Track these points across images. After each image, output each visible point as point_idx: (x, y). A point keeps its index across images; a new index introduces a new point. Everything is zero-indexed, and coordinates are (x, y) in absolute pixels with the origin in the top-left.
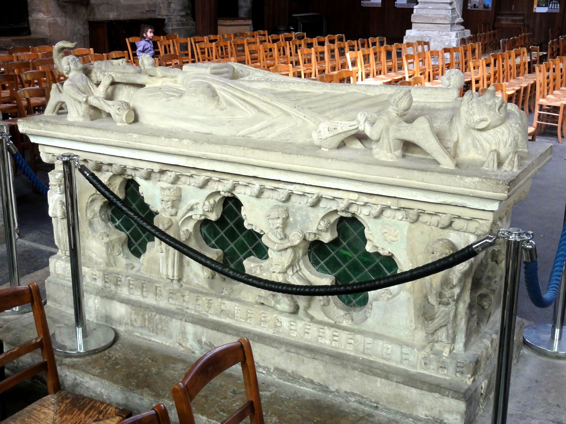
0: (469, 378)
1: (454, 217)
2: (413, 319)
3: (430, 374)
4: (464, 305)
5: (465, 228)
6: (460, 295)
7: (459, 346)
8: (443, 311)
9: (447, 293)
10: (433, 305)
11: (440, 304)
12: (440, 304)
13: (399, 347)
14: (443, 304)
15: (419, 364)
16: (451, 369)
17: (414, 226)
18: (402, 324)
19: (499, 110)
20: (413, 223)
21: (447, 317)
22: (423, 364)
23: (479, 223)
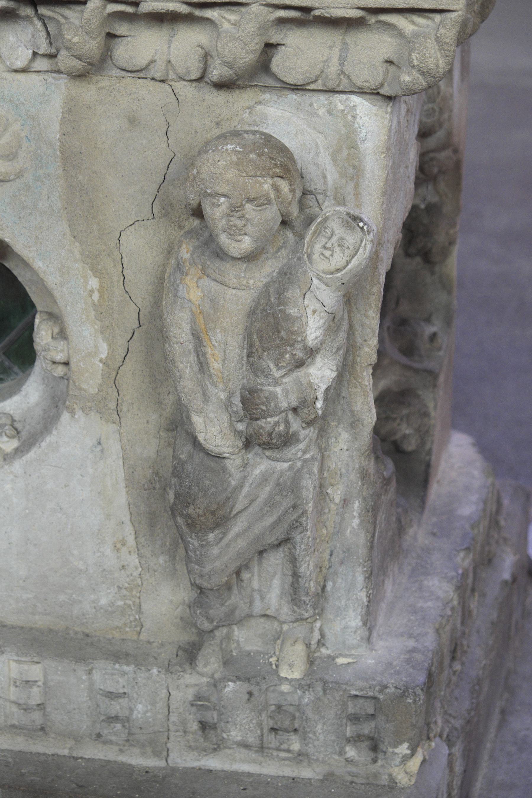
0: (405, 759)
1: (281, 21)
2: (129, 530)
3: (227, 767)
4: (355, 437)
5: (333, 68)
6: (336, 392)
7: (345, 622)
8: (264, 478)
9: (282, 390)
10: (219, 457)
11: (248, 445)
12: (248, 445)
14: (267, 446)
16: (322, 731)
17: (88, 92)
18: (81, 565)
20: (80, 76)
21: (286, 503)
22: (195, 726)
23: (400, 34)
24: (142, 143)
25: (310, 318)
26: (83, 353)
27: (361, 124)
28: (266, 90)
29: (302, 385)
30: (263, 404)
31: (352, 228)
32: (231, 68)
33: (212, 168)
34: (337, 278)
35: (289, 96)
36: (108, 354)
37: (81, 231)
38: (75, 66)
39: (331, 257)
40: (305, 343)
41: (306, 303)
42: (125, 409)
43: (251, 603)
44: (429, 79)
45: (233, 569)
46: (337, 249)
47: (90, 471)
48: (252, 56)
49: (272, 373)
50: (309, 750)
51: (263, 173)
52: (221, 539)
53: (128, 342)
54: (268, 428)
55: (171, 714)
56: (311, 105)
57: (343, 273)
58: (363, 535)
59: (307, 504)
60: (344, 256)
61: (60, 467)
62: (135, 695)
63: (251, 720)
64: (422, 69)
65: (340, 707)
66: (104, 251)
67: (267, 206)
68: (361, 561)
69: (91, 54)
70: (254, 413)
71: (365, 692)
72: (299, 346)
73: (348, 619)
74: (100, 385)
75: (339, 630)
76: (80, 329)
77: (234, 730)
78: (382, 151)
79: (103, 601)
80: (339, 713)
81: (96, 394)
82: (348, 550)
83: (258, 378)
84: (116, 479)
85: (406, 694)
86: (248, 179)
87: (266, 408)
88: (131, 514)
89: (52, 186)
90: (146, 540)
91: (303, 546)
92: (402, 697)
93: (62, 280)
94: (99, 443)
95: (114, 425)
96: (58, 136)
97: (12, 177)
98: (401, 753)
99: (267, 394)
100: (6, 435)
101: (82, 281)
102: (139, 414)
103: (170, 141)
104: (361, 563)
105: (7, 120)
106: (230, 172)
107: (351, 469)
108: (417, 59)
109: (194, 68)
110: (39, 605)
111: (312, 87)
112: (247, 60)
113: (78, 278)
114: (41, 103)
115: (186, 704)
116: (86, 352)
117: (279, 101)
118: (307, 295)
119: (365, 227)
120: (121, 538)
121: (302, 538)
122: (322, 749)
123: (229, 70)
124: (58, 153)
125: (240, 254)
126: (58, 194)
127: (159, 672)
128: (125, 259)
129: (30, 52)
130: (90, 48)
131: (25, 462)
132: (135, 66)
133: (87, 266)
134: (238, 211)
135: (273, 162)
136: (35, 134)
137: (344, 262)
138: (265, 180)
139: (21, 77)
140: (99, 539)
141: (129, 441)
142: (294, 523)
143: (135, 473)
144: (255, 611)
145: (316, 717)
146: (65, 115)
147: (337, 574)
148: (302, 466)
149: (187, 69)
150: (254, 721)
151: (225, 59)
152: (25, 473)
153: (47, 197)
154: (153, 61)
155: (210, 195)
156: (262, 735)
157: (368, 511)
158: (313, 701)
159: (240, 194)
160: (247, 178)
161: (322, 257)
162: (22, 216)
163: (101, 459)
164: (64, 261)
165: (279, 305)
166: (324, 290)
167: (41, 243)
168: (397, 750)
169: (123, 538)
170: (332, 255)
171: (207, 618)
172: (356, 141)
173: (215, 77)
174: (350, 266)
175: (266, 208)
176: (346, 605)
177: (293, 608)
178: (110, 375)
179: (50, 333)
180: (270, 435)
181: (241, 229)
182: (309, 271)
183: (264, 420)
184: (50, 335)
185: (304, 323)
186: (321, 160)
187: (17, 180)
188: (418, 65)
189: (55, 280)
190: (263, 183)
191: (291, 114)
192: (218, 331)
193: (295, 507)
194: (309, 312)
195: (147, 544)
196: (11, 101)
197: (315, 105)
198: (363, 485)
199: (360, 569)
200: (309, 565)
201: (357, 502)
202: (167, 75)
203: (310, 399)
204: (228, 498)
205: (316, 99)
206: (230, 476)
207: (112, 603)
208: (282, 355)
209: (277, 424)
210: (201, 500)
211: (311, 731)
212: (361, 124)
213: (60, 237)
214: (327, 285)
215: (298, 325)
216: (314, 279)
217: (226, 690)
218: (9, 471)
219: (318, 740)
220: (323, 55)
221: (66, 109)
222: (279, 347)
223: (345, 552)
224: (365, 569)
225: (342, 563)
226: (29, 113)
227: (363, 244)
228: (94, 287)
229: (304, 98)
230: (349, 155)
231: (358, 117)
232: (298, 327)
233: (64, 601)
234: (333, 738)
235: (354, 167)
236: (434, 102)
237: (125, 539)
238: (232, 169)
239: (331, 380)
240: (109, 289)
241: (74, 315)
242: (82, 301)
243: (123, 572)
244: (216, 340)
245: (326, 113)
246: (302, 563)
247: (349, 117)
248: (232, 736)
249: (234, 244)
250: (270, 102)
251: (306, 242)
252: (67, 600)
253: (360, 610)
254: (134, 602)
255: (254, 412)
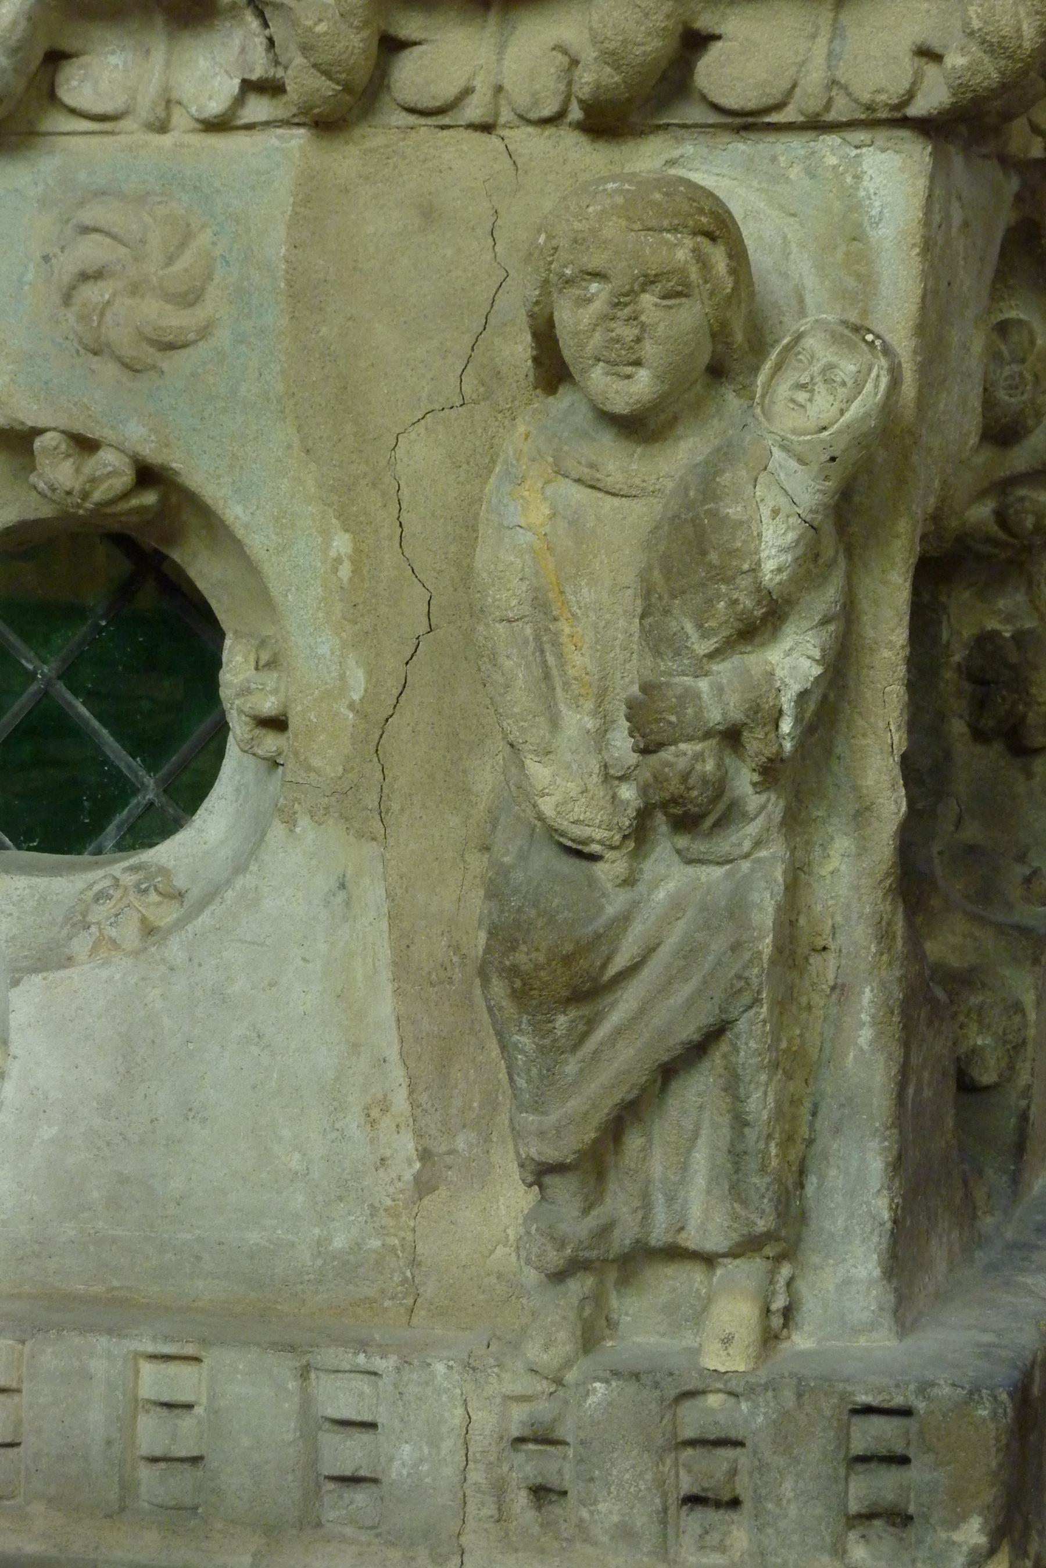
4: (862, 851)
5: (815, 77)
7: (847, 1271)
8: (676, 906)
13: (284, 1367)
15: (480, 1509)
17: (345, 159)
18: (295, 1162)
19: (785, 238)
21: (719, 945)
24: (445, 255)
25: (768, 524)
26: (317, 692)
27: (872, 191)
28: (686, 135)
29: (751, 676)
30: (672, 710)
31: (852, 347)
32: (617, 68)
33: (576, 223)
34: (822, 441)
35: (730, 146)
36: (366, 691)
37: (321, 438)
38: (318, 90)
39: (809, 404)
40: (756, 577)
41: (758, 493)
42: (395, 807)
43: (647, 1206)
44: (1003, 63)
45: (606, 1111)
46: (820, 387)
47: (323, 947)
48: (656, 43)
49: (689, 644)
50: (767, 1542)
51: (676, 222)
52: (584, 1036)
53: (407, 663)
54: (682, 764)
55: (471, 1465)
56: (774, 159)
57: (832, 430)
58: (881, 1066)
59: (761, 938)
60: (835, 400)
61: (261, 945)
62: (397, 1423)
63: (641, 1475)
64: (988, 38)
65: (832, 1434)
66: (365, 475)
67: (684, 300)
68: (877, 1124)
69: (352, 61)
70: (652, 732)
71: (888, 1397)
72: (744, 582)
73: (851, 1262)
74: (348, 758)
75: (831, 1288)
76: (311, 640)
77: (604, 1501)
78: (913, 241)
79: (339, 1242)
80: (830, 1448)
81: (340, 778)
82: (850, 1099)
83: (663, 659)
84: (374, 964)
85: (976, 1397)
86: (645, 236)
87: (678, 718)
88: (402, 1041)
89: (267, 351)
90: (430, 1097)
91: (753, 1044)
92: (967, 1403)
93: (280, 541)
94: (343, 886)
95: (374, 843)
96: (283, 250)
97: (191, 336)
98: (966, 1542)
99: (679, 691)
100: (156, 889)
101: (320, 540)
102: (424, 818)
103: (497, 248)
104: (877, 1130)
105: (188, 225)
106: (610, 224)
107: (855, 916)
108: (978, 17)
109: (548, 94)
110: (206, 1257)
111: (774, 118)
112: (648, 48)
113: (311, 535)
114: (253, 188)
115: (503, 1444)
116: (323, 689)
117: (710, 158)
118: (760, 480)
119: (878, 343)
120: (380, 1096)
121: (752, 1023)
122: (795, 1538)
123: (614, 73)
124: (282, 285)
125: (627, 403)
126: (278, 368)
127: (450, 1368)
128: (405, 491)
129: (237, 82)
130: (347, 47)
131: (191, 936)
132: (433, 97)
133: (331, 510)
134: (626, 305)
135: (695, 204)
136: (238, 249)
137: (834, 410)
138: (678, 239)
139: (219, 142)
140: (334, 1099)
141: (401, 878)
142: (735, 981)
143: (412, 948)
144: (654, 1235)
145: (781, 1461)
146: (298, 209)
147: (826, 1159)
148: (753, 870)
149: (533, 95)
150: (649, 1476)
151: (606, 45)
152: (190, 960)
153: (257, 374)
154: (467, 91)
155: (569, 282)
156: (665, 1510)
157: (892, 1013)
158: (774, 1421)
159: (629, 266)
160: (643, 233)
161: (791, 406)
162: (206, 414)
163: (345, 919)
164: (285, 502)
165: (704, 502)
166: (795, 472)
167: (241, 468)
168: (957, 1537)
169: (385, 1096)
170: (810, 400)
171: (552, 1238)
172: (861, 225)
173: (587, 89)
174: (848, 415)
175: (680, 305)
176: (846, 1229)
177: (733, 1208)
178: (367, 735)
179: (252, 658)
180: (685, 777)
181: (631, 348)
182: (765, 434)
183: (673, 748)
184: (253, 664)
185: (755, 534)
186: (794, 267)
187: (200, 344)
188: (980, 29)
189: (266, 542)
190: (675, 245)
191: (735, 182)
192: (583, 583)
193: (736, 947)
194: (765, 512)
195: (433, 1105)
196: (195, 187)
197: (782, 159)
198: (882, 954)
199: (874, 1144)
200: (765, 1093)
201: (867, 990)
202: (497, 115)
203: (767, 706)
204: (598, 936)
205: (783, 147)
206: (603, 895)
207: (357, 1244)
208: (709, 602)
209: (699, 757)
210: (542, 932)
211: (770, 1493)
212: (872, 191)
213: (280, 454)
214: (801, 461)
215: (743, 537)
216: (776, 451)
217: (589, 1402)
218: (158, 958)
219: (786, 1516)
220: (797, 53)
221: (300, 197)
222: (704, 585)
223: (843, 1105)
224: (886, 1144)
225: (837, 1131)
226: (230, 210)
227: (873, 375)
228: (343, 551)
229: (761, 146)
230: (847, 254)
231: (866, 178)
232: (744, 541)
233: (258, 1244)
234: (819, 1511)
235: (859, 277)
236: (1023, 361)
237: (389, 1097)
238: (614, 218)
239: (812, 679)
240: (372, 555)
241: (302, 612)
242: (319, 582)
243: (381, 1173)
244: (578, 602)
245: (802, 175)
246: (752, 1086)
247: (849, 180)
248: (599, 1513)
249: (619, 385)
250: (694, 160)
251: (759, 383)
252: (264, 1243)
253: (875, 1239)
254: (404, 1238)
255: (651, 729)
